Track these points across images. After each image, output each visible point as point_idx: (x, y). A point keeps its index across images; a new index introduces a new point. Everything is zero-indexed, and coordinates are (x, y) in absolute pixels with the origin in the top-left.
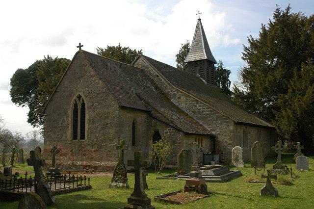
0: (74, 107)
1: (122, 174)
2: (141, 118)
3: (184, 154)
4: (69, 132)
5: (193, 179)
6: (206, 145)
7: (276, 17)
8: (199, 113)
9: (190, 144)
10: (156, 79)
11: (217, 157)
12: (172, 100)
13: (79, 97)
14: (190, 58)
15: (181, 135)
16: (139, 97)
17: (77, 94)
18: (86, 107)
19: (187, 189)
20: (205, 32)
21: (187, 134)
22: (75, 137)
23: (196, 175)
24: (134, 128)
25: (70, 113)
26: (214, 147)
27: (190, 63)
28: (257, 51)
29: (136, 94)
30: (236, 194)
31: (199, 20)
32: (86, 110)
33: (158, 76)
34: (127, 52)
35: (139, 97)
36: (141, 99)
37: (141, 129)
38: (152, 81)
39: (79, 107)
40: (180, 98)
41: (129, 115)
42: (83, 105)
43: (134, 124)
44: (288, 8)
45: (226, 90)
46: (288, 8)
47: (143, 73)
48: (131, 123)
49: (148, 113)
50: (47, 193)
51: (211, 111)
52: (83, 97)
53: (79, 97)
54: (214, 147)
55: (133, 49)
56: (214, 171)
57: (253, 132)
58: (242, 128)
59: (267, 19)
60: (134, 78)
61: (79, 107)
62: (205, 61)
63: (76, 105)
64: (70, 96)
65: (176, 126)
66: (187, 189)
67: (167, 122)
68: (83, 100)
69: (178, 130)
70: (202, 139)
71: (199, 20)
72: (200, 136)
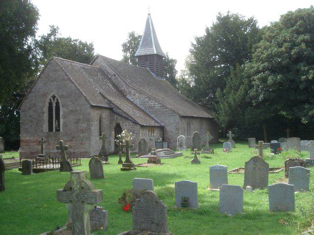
0: (49, 105)
1: (104, 156)
2: (105, 114)
3: (142, 142)
4: (45, 127)
5: (152, 156)
6: (157, 134)
7: (219, 18)
8: (150, 107)
9: (144, 135)
10: (113, 78)
11: (165, 144)
12: (129, 97)
13: (54, 97)
14: (140, 52)
15: (138, 127)
16: (103, 96)
17: (52, 94)
18: (60, 105)
19: (149, 162)
20: (155, 29)
21: (142, 126)
22: (51, 129)
23: (155, 154)
24: (100, 121)
25: (46, 110)
26: (163, 136)
27: (140, 57)
28: (205, 48)
29: (100, 93)
30: (205, 218)
31: (149, 14)
32: (61, 108)
33: (115, 75)
34: (78, 43)
35: (103, 96)
36: (105, 98)
37: (106, 122)
38: (110, 79)
39: (54, 105)
40: (134, 95)
41: (97, 112)
42: (57, 103)
43: (100, 119)
44: (229, 12)
45: (173, 81)
46: (229, 12)
47: (101, 71)
48: (99, 118)
49: (111, 109)
50: (69, 165)
51: (161, 107)
52: (57, 96)
53: (54, 97)
54: (163, 136)
55: (84, 41)
56: (164, 153)
57: (195, 125)
58: (186, 120)
59: (211, 21)
60: (95, 78)
61: (54, 105)
62: (155, 58)
63: (50, 104)
64: (45, 95)
65: (134, 120)
66: (149, 162)
67: (127, 116)
68: (57, 100)
69: (136, 123)
70: (154, 130)
71: (149, 14)
72: (151, 128)
